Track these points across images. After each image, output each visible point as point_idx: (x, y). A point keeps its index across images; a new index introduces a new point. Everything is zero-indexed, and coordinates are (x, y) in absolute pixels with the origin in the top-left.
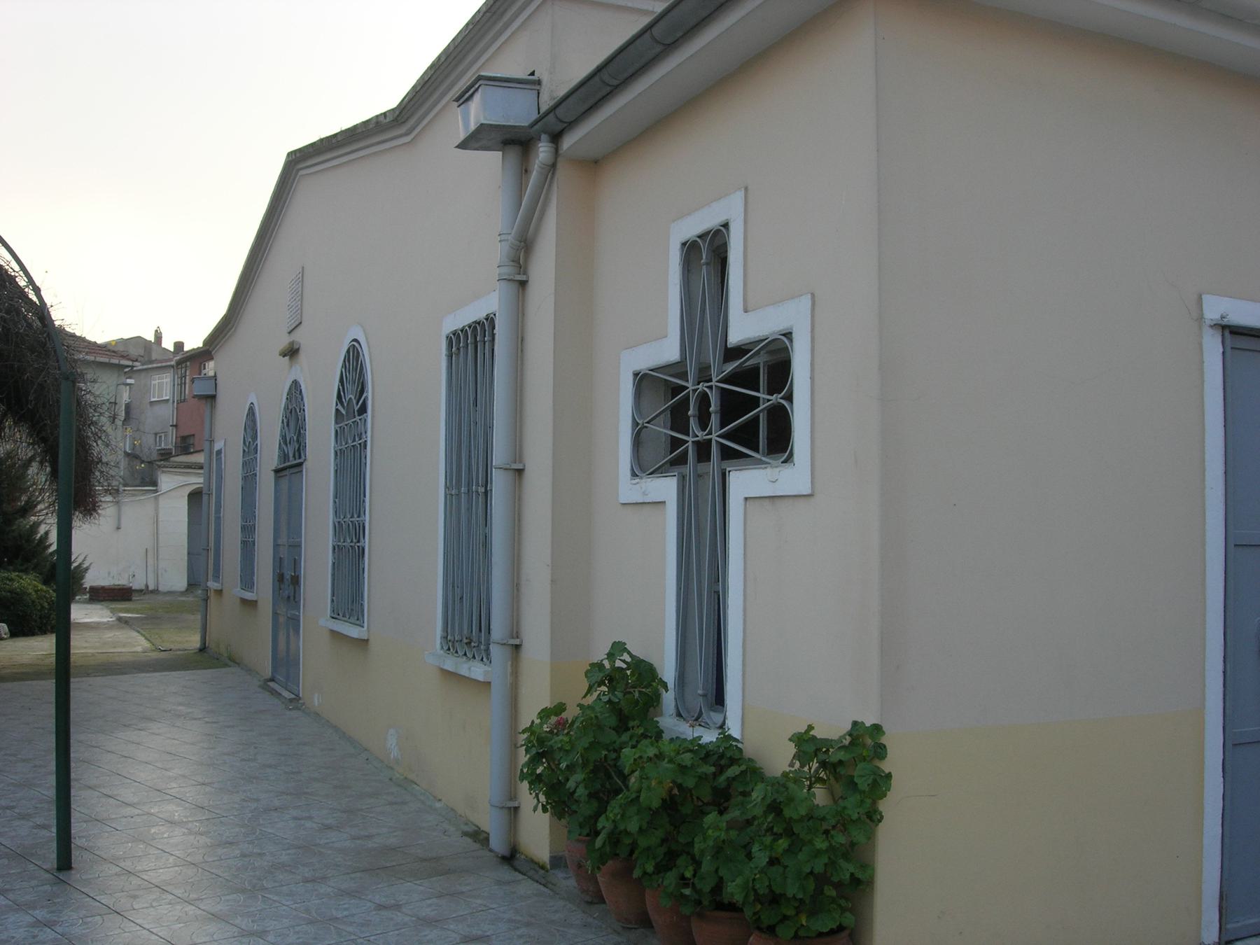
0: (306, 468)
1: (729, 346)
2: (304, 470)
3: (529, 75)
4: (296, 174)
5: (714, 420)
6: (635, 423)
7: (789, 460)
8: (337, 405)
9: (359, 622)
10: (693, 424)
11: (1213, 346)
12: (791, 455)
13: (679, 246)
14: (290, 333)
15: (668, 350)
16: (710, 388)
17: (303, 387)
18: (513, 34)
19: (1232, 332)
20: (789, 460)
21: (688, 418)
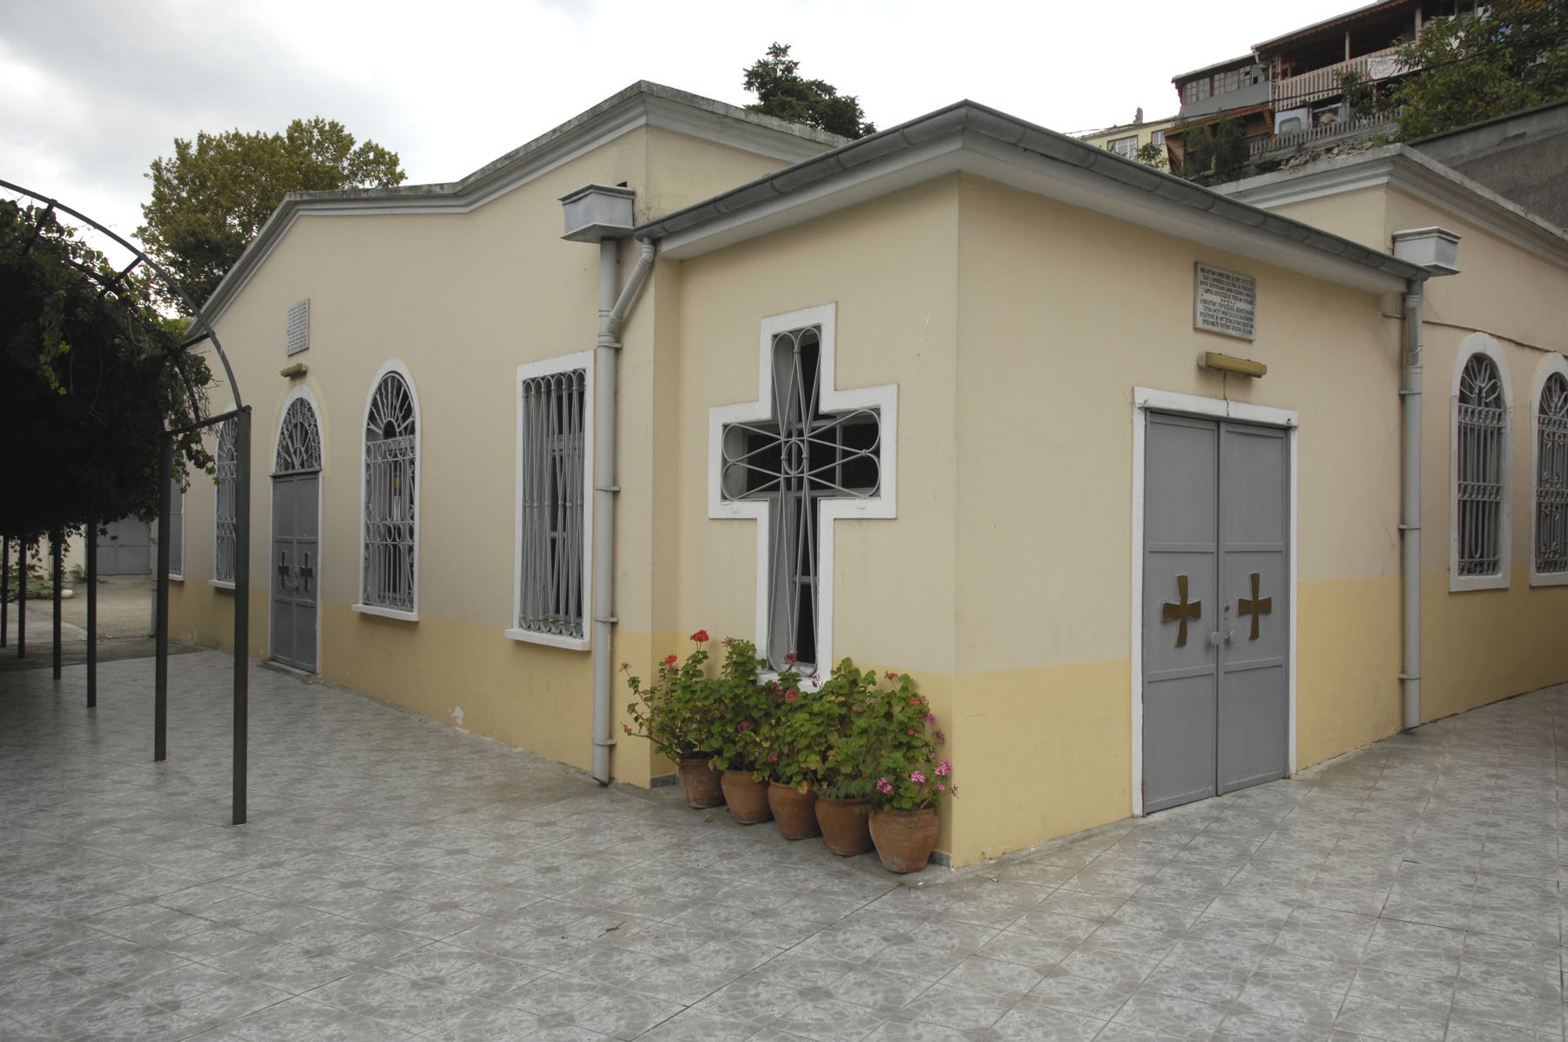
0: (323, 478)
1: (820, 412)
2: (320, 479)
3: (619, 185)
4: (296, 213)
5: (805, 463)
6: (725, 461)
7: (876, 494)
8: (368, 424)
9: (408, 603)
10: (784, 464)
11: (1139, 420)
12: (878, 488)
13: (770, 337)
14: (290, 356)
15: (759, 410)
16: (803, 441)
17: (314, 406)
18: (600, 147)
19: (1151, 412)
20: (876, 494)
21: (781, 461)
